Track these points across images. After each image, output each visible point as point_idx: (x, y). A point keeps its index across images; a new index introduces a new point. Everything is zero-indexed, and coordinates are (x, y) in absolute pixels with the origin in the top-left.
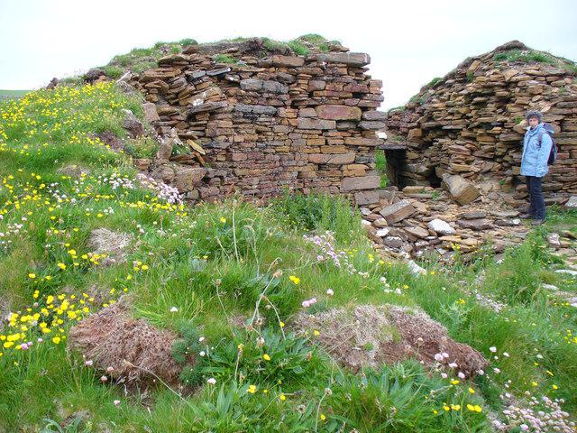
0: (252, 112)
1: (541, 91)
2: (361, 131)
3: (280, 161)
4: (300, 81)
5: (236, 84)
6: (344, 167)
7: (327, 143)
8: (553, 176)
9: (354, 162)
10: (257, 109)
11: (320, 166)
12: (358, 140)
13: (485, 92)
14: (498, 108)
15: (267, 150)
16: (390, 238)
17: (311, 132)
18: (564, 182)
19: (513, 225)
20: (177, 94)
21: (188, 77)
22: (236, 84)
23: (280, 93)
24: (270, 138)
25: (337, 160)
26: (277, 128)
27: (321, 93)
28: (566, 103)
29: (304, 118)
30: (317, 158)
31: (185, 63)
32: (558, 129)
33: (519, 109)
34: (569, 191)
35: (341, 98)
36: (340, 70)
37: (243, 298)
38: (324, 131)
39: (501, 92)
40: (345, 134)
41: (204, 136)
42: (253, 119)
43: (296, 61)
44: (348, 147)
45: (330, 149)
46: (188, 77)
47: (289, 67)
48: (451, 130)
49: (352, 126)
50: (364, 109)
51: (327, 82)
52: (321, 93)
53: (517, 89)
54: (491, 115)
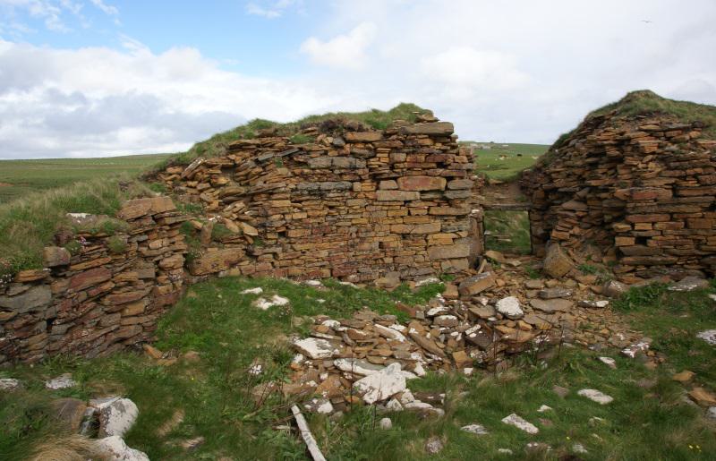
0: (319, 189)
1: (655, 149)
2: (449, 202)
3: (357, 232)
4: (378, 155)
5: (305, 164)
6: (429, 237)
7: (409, 214)
8: (664, 249)
9: (441, 231)
10: (325, 186)
11: (404, 236)
12: (444, 210)
13: (597, 152)
14: (609, 169)
15: (340, 224)
16: (443, 317)
17: (391, 203)
18: (680, 256)
19: (596, 308)
20: (247, 175)
21: (257, 162)
22: (305, 164)
23: (355, 168)
24: (343, 212)
25: (420, 230)
26: (350, 202)
27: (402, 165)
28: (677, 164)
29: (387, 192)
30: (399, 228)
31: (254, 147)
32: (670, 193)
33: (627, 171)
34: (685, 266)
35: (424, 169)
36: (420, 142)
37: (574, 261)
38: (405, 202)
39: (614, 152)
40: (431, 204)
41: (258, 216)
42: (321, 195)
43: (374, 136)
44: (435, 217)
45: (412, 220)
46: (257, 162)
47: (365, 142)
48: (566, 193)
49: (438, 196)
50: (449, 179)
51: (407, 154)
52: (402, 165)
53: (629, 149)
54: (598, 178)
